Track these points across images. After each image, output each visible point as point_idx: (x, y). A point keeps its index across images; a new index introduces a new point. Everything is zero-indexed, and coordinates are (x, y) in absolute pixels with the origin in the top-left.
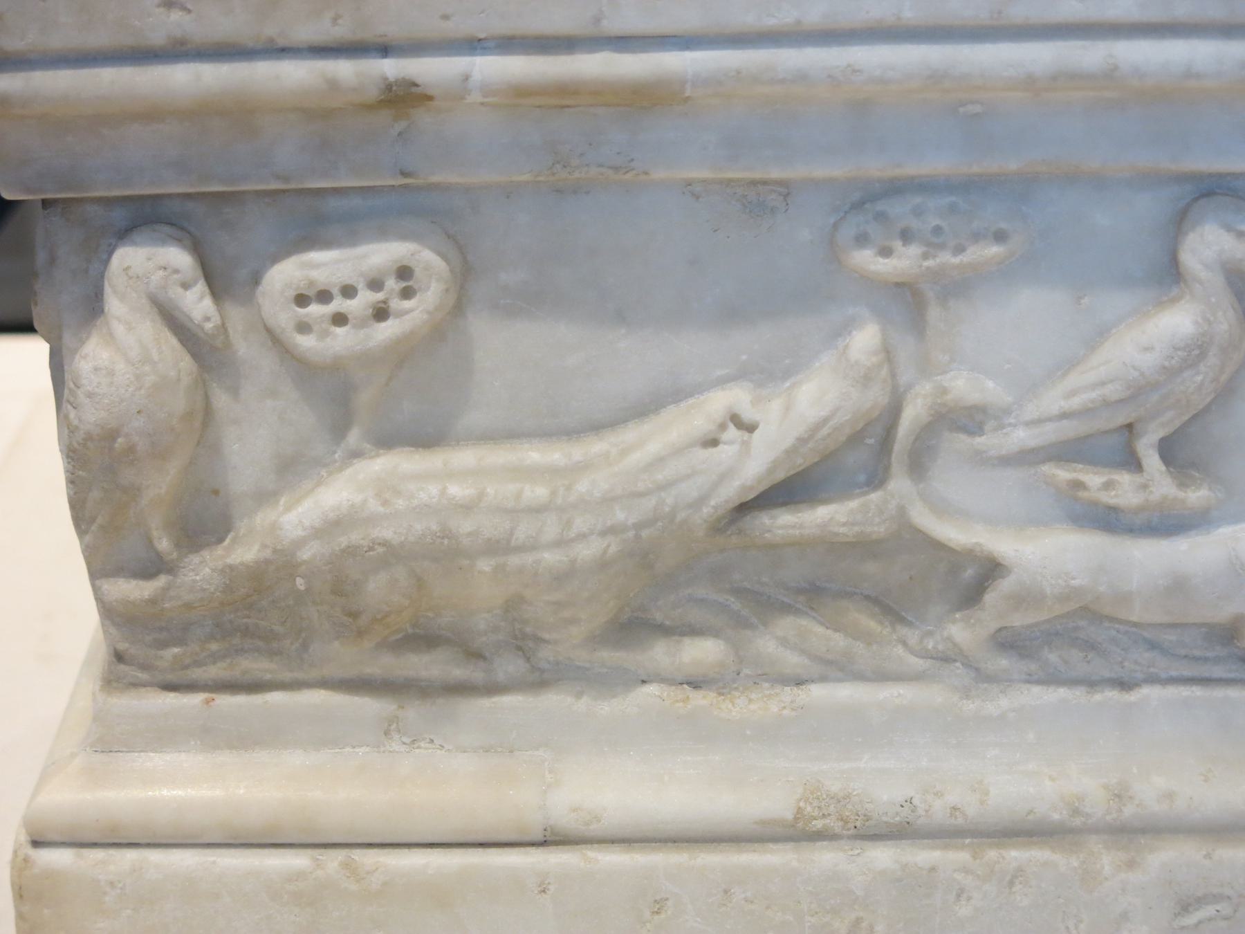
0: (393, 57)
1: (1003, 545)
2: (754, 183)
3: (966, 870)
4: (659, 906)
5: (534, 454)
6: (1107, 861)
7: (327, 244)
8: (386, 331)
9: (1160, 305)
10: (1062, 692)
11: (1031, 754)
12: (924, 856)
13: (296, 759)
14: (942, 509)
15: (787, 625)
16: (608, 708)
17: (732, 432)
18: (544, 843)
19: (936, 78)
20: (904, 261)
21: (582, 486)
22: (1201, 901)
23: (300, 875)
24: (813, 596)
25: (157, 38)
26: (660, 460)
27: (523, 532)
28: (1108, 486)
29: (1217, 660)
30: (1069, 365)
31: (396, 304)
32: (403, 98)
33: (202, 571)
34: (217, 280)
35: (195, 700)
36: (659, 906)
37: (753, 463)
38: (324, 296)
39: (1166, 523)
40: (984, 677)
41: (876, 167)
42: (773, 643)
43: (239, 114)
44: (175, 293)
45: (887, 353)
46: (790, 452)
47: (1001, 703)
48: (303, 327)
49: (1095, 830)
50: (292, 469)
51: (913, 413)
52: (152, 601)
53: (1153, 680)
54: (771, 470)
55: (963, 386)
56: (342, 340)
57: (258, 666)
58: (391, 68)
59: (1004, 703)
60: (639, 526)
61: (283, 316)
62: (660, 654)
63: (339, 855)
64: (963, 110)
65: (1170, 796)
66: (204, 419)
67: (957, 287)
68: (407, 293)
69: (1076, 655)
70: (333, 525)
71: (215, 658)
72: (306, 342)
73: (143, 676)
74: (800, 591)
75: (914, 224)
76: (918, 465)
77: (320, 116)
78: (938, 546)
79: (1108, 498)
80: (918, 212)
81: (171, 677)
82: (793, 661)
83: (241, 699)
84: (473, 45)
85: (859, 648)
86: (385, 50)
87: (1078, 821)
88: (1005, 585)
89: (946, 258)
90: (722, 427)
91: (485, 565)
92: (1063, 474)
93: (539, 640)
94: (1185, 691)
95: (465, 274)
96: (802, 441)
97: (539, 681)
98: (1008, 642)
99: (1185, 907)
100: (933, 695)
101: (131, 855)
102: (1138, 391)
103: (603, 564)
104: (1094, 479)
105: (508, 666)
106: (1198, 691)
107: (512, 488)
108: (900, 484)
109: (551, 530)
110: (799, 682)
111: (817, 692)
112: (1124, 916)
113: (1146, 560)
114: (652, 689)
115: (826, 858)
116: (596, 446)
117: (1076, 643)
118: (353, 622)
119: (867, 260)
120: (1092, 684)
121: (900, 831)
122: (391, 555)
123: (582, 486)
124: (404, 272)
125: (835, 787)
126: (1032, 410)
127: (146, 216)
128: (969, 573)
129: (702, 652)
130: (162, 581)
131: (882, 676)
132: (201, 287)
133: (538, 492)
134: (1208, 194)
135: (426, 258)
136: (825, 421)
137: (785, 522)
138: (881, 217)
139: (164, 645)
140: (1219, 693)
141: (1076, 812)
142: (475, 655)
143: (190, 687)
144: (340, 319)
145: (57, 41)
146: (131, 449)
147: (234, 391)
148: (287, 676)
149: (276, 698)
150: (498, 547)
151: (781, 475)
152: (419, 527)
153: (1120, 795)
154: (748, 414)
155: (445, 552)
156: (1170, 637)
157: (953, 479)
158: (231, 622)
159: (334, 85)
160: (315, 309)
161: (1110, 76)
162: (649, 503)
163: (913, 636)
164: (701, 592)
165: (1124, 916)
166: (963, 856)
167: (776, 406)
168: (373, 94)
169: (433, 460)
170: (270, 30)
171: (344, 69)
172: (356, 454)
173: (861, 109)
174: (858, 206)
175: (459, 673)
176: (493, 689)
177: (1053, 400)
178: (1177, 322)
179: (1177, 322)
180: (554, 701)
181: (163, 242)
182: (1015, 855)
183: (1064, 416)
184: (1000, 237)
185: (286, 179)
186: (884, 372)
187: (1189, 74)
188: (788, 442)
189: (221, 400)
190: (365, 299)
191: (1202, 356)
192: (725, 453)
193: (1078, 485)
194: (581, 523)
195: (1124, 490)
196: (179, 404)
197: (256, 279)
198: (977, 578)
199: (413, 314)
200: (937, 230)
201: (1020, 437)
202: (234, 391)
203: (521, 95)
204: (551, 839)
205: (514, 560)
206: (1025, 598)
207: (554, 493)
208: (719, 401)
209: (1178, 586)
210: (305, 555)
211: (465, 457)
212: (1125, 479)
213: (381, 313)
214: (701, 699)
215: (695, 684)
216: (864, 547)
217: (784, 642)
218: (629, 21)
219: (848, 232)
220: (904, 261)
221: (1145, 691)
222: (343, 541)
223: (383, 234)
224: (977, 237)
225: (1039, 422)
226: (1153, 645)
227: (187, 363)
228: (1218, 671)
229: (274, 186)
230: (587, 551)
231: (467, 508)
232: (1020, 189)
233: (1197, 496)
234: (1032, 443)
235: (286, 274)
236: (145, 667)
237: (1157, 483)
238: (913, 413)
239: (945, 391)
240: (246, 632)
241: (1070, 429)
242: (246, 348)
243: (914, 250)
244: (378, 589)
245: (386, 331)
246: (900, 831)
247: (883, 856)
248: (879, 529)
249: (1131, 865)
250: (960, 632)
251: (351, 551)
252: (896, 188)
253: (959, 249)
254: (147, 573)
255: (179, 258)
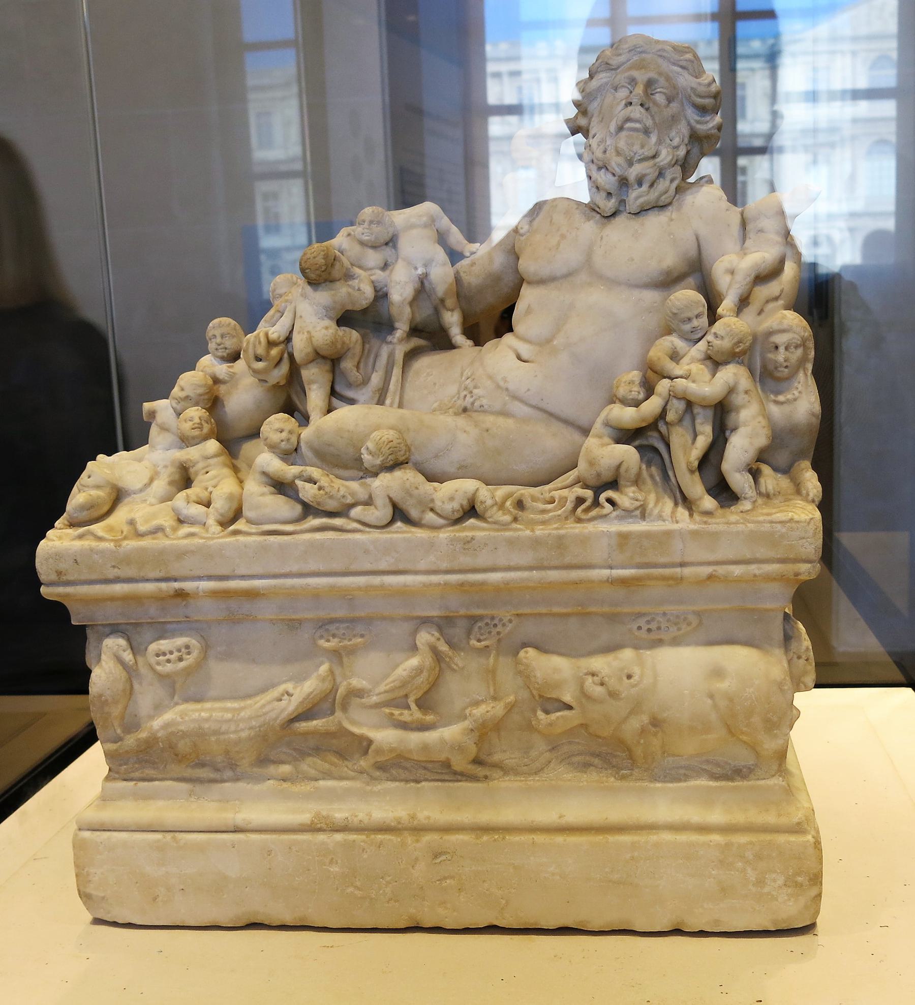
0: (688, 645)
1: (373, 734)
2: (290, 620)
3: (364, 841)
4: (270, 852)
5: (229, 705)
6: (409, 839)
7: (165, 638)
8: (182, 665)
9: (413, 656)
10: (397, 784)
11: (386, 804)
12: (352, 837)
13: (160, 803)
14: (353, 722)
15: (309, 760)
16: (258, 787)
17: (286, 697)
18: (235, 831)
19: (332, 588)
20: (333, 644)
21: (242, 714)
22: (441, 854)
23: (159, 841)
24: (317, 751)
25: (111, 576)
26: (264, 706)
27: (224, 727)
28: (401, 714)
29: (446, 773)
30: (387, 676)
31: (185, 656)
32: (181, 594)
33: (130, 741)
34: (134, 649)
35: (131, 784)
36: (270, 852)
37: (290, 706)
38: (164, 654)
39: (423, 727)
40: (373, 778)
41: (323, 614)
42: (308, 765)
43: (136, 599)
44: (121, 652)
45: (331, 672)
46: (302, 703)
47: (379, 787)
48: (158, 664)
49: (406, 829)
50: (159, 708)
51: (341, 691)
52: (116, 750)
53: (426, 780)
54: (297, 708)
55: (356, 682)
56: (169, 667)
57: (150, 772)
58: (176, 585)
59: (379, 787)
60: (260, 727)
61: (153, 660)
62: (272, 769)
63: (172, 834)
64: (347, 596)
65: (429, 818)
66: (130, 692)
67: (352, 651)
68: (189, 653)
69: (401, 771)
70: (166, 726)
71: (137, 770)
72: (159, 668)
73: (117, 776)
74: (313, 749)
75: (336, 632)
76: (345, 708)
77: (159, 598)
78: (353, 734)
79: (402, 718)
80: (337, 629)
81: (125, 777)
82: (313, 772)
83: (146, 784)
84: (200, 578)
85: (333, 768)
86: (176, 580)
87: (400, 826)
88: (373, 747)
89: (346, 643)
90: (283, 695)
91: (213, 739)
92: (387, 710)
93: (237, 765)
94: (436, 784)
95: (206, 648)
96: (305, 699)
97: (237, 779)
98: (381, 767)
99: (436, 856)
100: (356, 784)
101: (108, 833)
102: (404, 684)
103: (250, 739)
104: (396, 712)
105: (228, 774)
106: (440, 784)
107: (220, 714)
108: (339, 714)
109: (233, 728)
110: (316, 780)
111: (322, 783)
112: (417, 859)
113: (415, 738)
114: (271, 782)
115: (321, 837)
116: (249, 702)
117: (399, 767)
118: (179, 758)
119: (322, 643)
120: (407, 781)
121: (344, 828)
122: (184, 735)
123: (242, 714)
124: (187, 647)
125: (324, 813)
126: (377, 691)
127: (115, 630)
128: (365, 744)
129: (286, 769)
130: (119, 744)
131: (341, 778)
132: (129, 651)
133: (229, 716)
134: (424, 623)
135: (193, 642)
136: (312, 693)
137: (303, 726)
138: (327, 630)
139: (121, 765)
140: (447, 784)
141: (399, 823)
142: (217, 770)
143: (131, 780)
144: (169, 661)
145: (83, 577)
146: (107, 700)
147: (141, 684)
148: (160, 776)
149: (157, 783)
150: (216, 732)
151: (300, 710)
152: (192, 726)
153: (413, 817)
154: (291, 691)
155: (199, 735)
156: (430, 766)
157: (355, 713)
158: (774, 881)
159: (160, 590)
160: (161, 658)
161: (382, 587)
162: (262, 719)
163: (350, 764)
164: (284, 750)
165: (417, 859)
166: (364, 837)
167: (299, 689)
168: (172, 593)
169: (198, 706)
170: (142, 574)
171: (163, 585)
172: (177, 704)
173: (316, 596)
174: (321, 627)
175: (212, 775)
176: (223, 781)
177: (382, 688)
178: (414, 662)
179: (414, 662)
180: (241, 785)
181: (118, 637)
182: (380, 837)
183: (386, 692)
184: (362, 636)
185: (152, 619)
186: (330, 678)
187: (405, 586)
188: (301, 699)
189: (136, 686)
190: (176, 654)
191: (422, 672)
192: (283, 703)
193: (392, 714)
194: (241, 726)
195: (406, 716)
196: (120, 686)
197: (146, 649)
198: (365, 745)
199: (189, 660)
200: (344, 634)
201: (375, 699)
202: (141, 684)
203: (215, 594)
204: (237, 830)
205: (222, 737)
206: (379, 751)
207: (234, 716)
208: (282, 688)
209: (425, 748)
210: (159, 735)
211: (208, 705)
212: (406, 712)
213: (180, 659)
214: (285, 785)
215: (284, 780)
216: (328, 734)
217: (309, 766)
218: (242, 571)
219: (318, 634)
220: (333, 644)
221: (423, 783)
222: (170, 730)
223: (181, 635)
224: (355, 636)
225: (380, 694)
226: (425, 768)
227: (124, 674)
228: (447, 777)
229: (149, 621)
230: (244, 735)
231: (207, 720)
232: (369, 620)
233: (430, 718)
234: (378, 701)
235: (153, 647)
236: (117, 773)
237: (414, 714)
238: (341, 691)
239: (350, 684)
240: (146, 761)
241: (389, 696)
242: (143, 670)
243: (336, 640)
244: (183, 746)
245: (182, 665)
246: (344, 828)
247: (339, 837)
248: (333, 729)
249: (417, 841)
250: (363, 763)
251: (172, 733)
252: (332, 621)
253: (350, 640)
254: (115, 742)
255: (122, 642)
